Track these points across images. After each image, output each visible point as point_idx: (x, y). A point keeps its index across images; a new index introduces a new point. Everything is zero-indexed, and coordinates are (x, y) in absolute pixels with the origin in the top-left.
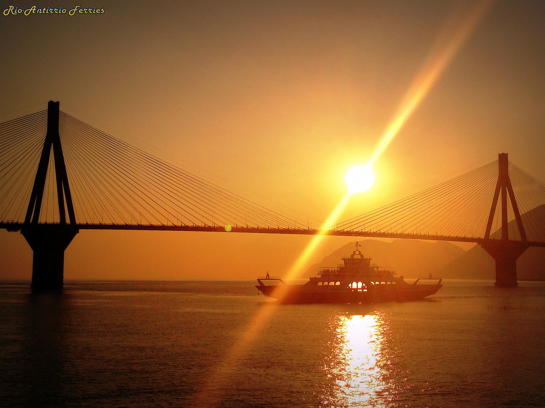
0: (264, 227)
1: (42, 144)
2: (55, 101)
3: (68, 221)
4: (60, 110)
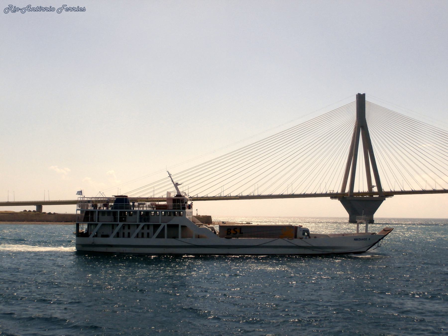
2: (362, 93)
3: (375, 189)
4: (366, 100)
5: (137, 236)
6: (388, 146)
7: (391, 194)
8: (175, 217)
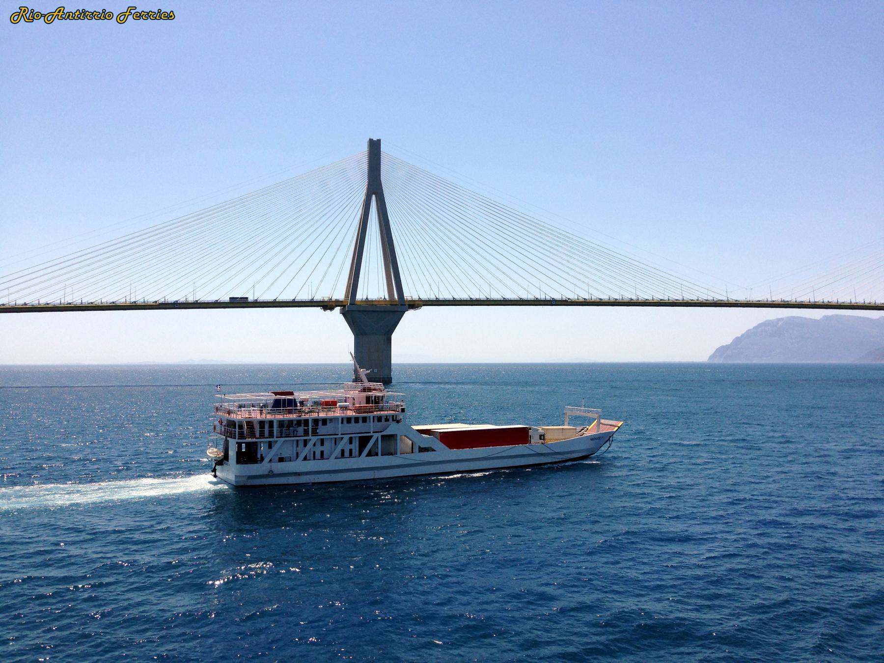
0: (617, 297)
1: (362, 195)
3: (396, 296)
5: (305, 459)
6: (458, 241)
7: (415, 305)
8: (349, 425)
